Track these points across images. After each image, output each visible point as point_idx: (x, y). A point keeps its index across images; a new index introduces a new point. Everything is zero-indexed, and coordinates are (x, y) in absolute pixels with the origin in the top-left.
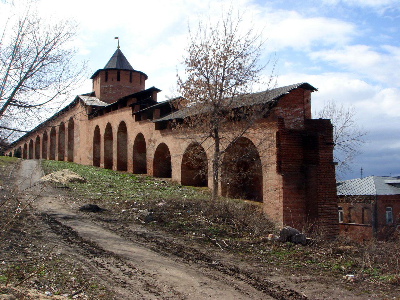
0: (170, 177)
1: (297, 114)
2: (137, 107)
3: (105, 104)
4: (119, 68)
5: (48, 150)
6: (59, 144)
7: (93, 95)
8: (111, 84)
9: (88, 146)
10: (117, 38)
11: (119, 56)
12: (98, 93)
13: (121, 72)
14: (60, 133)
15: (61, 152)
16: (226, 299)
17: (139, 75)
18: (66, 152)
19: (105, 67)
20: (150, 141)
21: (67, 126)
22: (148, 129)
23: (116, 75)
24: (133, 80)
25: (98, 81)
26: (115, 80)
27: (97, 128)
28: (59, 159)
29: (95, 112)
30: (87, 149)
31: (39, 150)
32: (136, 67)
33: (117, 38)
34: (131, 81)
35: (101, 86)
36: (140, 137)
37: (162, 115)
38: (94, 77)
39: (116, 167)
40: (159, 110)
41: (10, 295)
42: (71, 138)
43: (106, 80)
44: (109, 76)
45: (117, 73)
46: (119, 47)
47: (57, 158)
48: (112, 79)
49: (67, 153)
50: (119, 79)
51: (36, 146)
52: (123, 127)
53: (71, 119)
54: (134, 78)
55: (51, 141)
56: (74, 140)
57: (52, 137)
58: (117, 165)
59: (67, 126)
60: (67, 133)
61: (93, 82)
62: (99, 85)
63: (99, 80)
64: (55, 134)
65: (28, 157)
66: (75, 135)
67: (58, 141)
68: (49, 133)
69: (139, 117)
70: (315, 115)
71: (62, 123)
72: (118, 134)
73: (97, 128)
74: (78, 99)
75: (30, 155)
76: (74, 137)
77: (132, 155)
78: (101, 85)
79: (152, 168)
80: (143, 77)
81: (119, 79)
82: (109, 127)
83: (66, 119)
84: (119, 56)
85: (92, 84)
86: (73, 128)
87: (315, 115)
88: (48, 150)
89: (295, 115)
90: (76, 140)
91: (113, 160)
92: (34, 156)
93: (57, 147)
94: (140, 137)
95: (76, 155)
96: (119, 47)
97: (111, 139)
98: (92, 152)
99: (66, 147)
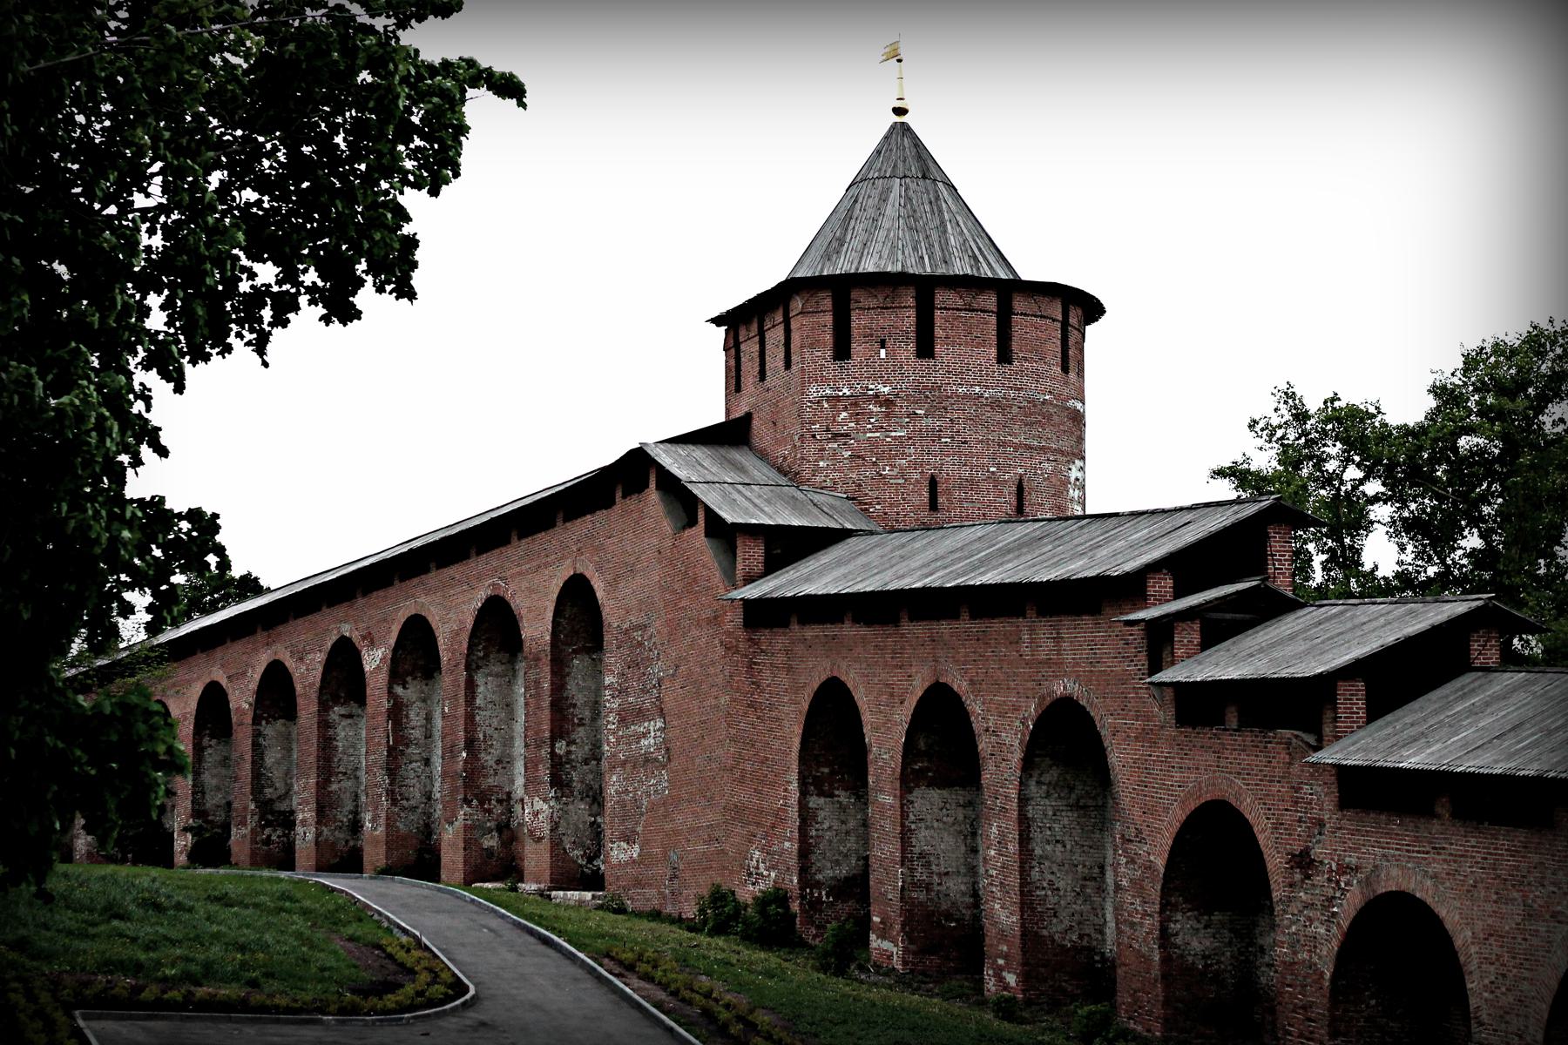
13: (942, 297)
23: (909, 319)
44: (858, 322)
45: (911, 302)
57: (399, 690)
81: (925, 348)
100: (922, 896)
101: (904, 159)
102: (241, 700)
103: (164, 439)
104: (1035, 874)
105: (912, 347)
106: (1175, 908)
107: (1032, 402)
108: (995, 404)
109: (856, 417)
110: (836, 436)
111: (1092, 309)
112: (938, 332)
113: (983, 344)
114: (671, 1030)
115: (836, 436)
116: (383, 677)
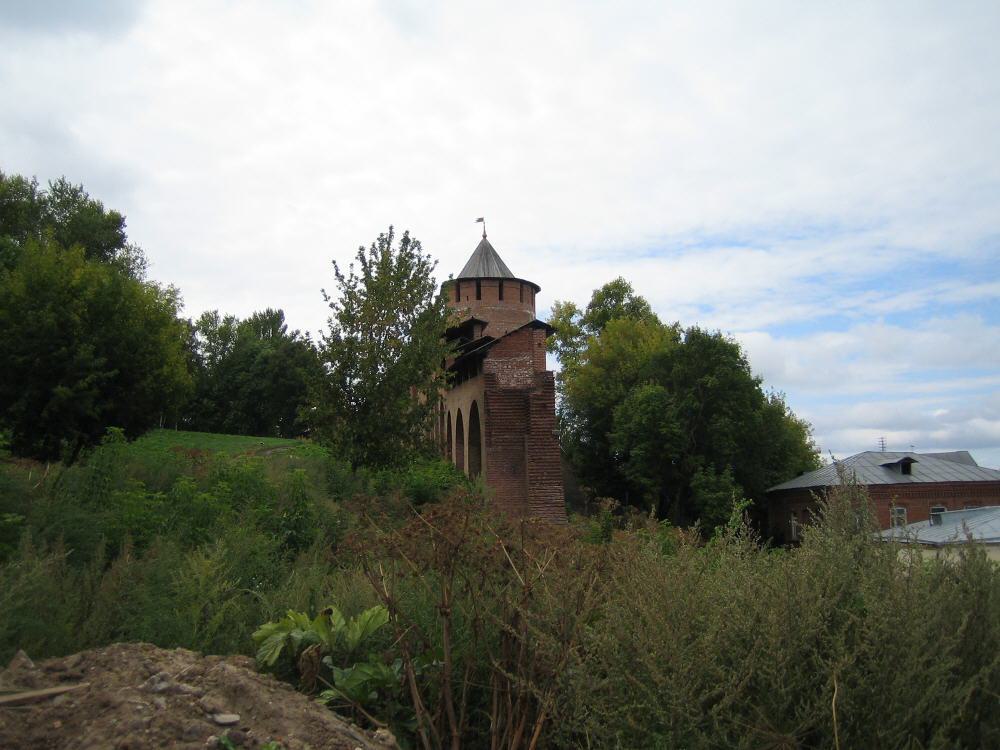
1: (521, 365)
10: (481, 220)
11: (485, 252)
16: (635, 748)
24: (504, 295)
32: (519, 272)
33: (481, 220)
34: (501, 298)
41: (532, 628)
44: (505, 290)
46: (485, 236)
50: (479, 297)
54: (507, 292)
70: (548, 369)
80: (530, 289)
81: (479, 297)
84: (485, 252)
87: (548, 369)
89: (519, 367)
96: (485, 236)
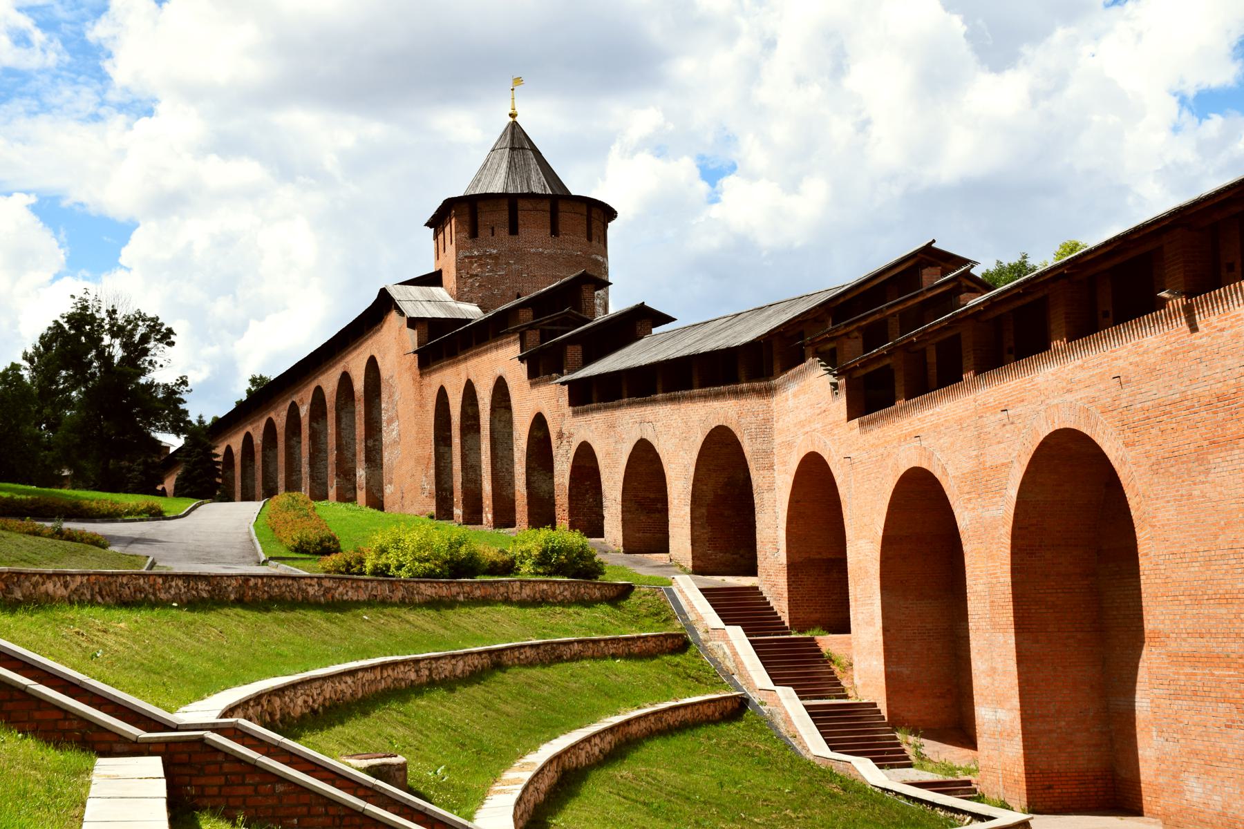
0: (667, 551)
2: (533, 337)
3: (471, 311)
4: (511, 190)
5: (305, 469)
6: (339, 447)
7: (434, 279)
8: (497, 243)
9: (420, 452)
12: (450, 277)
13: (521, 204)
14: (339, 409)
15: (346, 473)
17: (584, 209)
18: (361, 473)
19: (472, 186)
20: (560, 435)
21: (359, 385)
22: (554, 401)
23: (505, 216)
25: (447, 229)
26: (503, 232)
27: (442, 394)
28: (341, 498)
29: (441, 343)
30: (418, 461)
31: (276, 470)
35: (457, 253)
36: (539, 422)
37: (588, 360)
38: (437, 222)
39: (490, 516)
40: (579, 347)
42: (373, 428)
43: (474, 234)
44: (482, 219)
45: (506, 207)
47: (332, 492)
48: (493, 229)
49: (363, 477)
50: (514, 230)
51: (264, 456)
52: (501, 390)
53: (372, 362)
55: (316, 437)
56: (384, 434)
57: (315, 425)
58: (494, 509)
59: (359, 385)
60: (360, 408)
61: (436, 237)
62: (451, 249)
63: (451, 229)
64: (324, 414)
65: (238, 495)
66: (384, 417)
67: (460, 474)
68: (304, 411)
69: (541, 366)
71: (294, 403)
72: (492, 414)
73: (442, 394)
74: (384, 304)
75: (244, 487)
76: (384, 424)
77: (524, 477)
78: (458, 248)
79: (566, 514)
81: (514, 230)
82: (470, 392)
83: (329, 382)
85: (433, 243)
86: (379, 395)
88: (305, 469)
90: (389, 433)
91: (484, 495)
92: (259, 489)
93: (332, 457)
94: (539, 422)
95: (390, 483)
97: (477, 429)
98: (432, 472)
99: (361, 456)
100: (472, 486)
101: (517, 142)
102: (258, 440)
103: (57, 283)
104: (499, 465)
105: (507, 230)
106: (534, 469)
107: (571, 255)
108: (550, 257)
109: (481, 266)
110: (472, 276)
111: (609, 213)
112: (520, 222)
113: (1153, 632)
114: (206, 561)
115: (472, 276)
116: (307, 419)
